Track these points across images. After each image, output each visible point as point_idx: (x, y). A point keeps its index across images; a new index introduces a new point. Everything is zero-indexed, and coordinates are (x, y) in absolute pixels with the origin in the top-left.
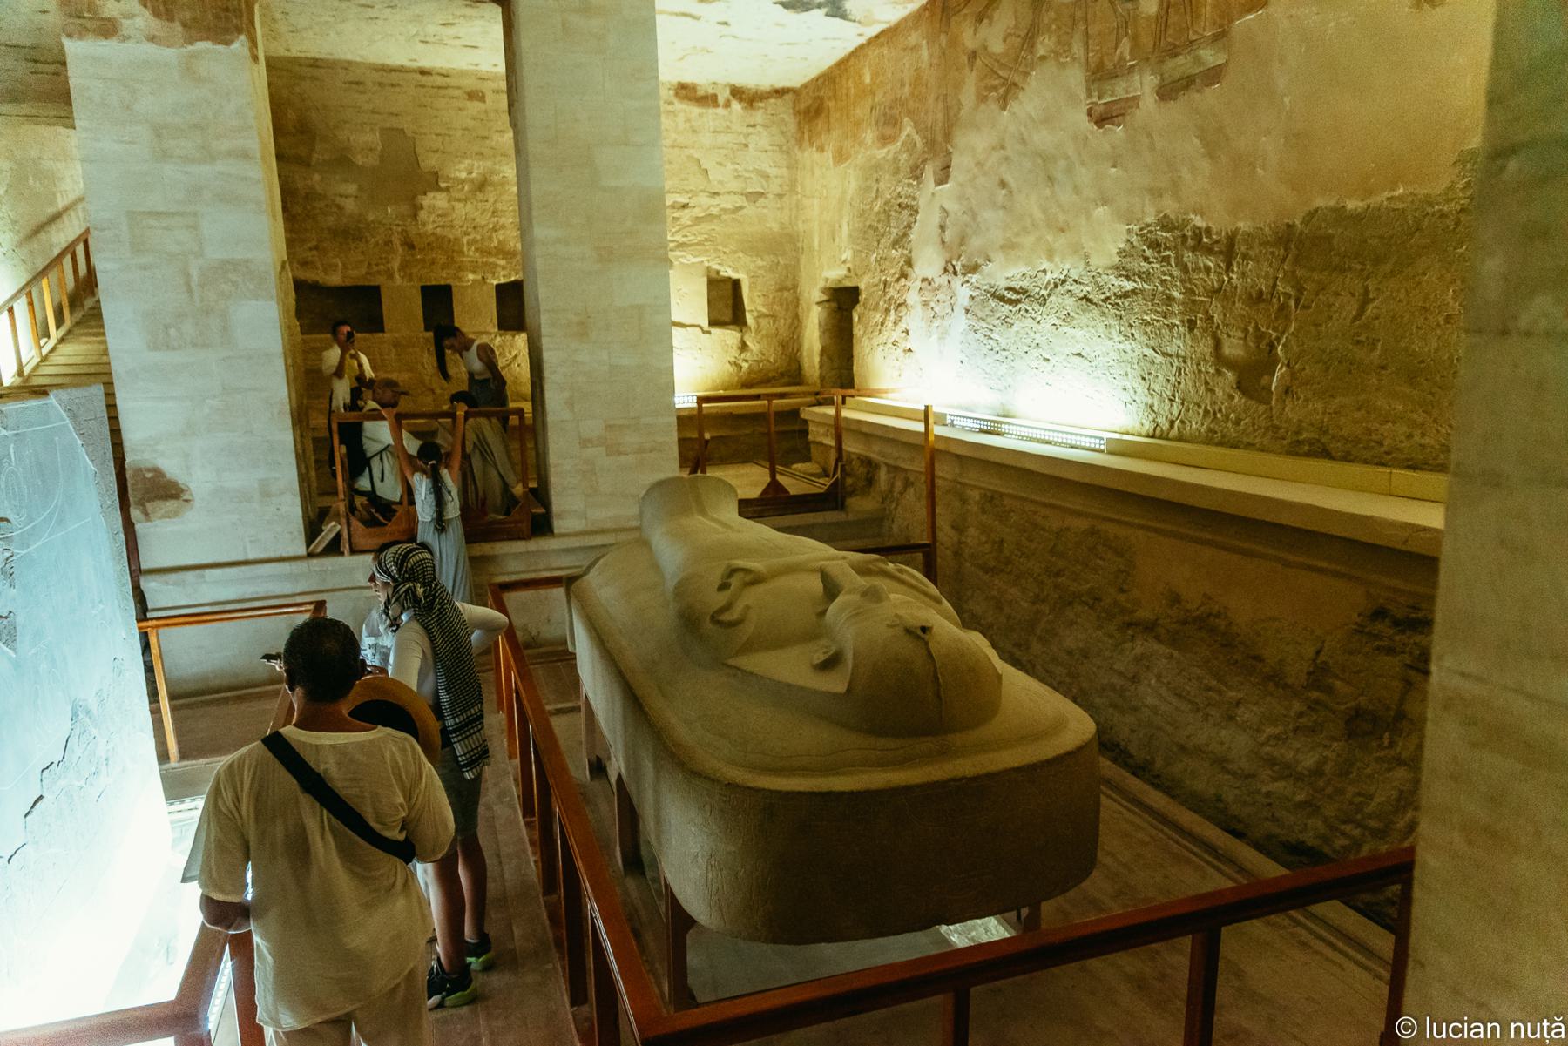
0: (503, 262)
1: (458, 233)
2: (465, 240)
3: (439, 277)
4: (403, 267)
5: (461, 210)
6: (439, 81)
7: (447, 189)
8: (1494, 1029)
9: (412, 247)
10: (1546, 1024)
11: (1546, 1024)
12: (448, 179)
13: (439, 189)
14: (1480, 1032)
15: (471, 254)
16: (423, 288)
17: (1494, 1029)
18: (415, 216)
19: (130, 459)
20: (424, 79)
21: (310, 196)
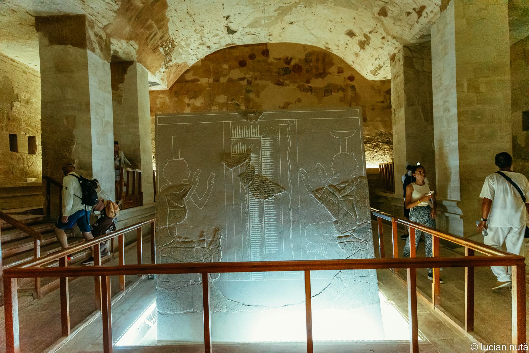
0: (31, 129)
1: (21, 117)
2: (23, 120)
3: (14, 132)
4: (6, 126)
5: (23, 109)
6: (16, 64)
7: (20, 101)
8: (504, 347)
9: (9, 119)
10: (521, 346)
11: (521, 346)
12: (21, 98)
13: (18, 101)
14: (499, 348)
15: (23, 125)
16: (10, 135)
17: (504, 347)
18: (11, 109)
19: (228, 277)
20: (12, 62)
21: (380, 197)
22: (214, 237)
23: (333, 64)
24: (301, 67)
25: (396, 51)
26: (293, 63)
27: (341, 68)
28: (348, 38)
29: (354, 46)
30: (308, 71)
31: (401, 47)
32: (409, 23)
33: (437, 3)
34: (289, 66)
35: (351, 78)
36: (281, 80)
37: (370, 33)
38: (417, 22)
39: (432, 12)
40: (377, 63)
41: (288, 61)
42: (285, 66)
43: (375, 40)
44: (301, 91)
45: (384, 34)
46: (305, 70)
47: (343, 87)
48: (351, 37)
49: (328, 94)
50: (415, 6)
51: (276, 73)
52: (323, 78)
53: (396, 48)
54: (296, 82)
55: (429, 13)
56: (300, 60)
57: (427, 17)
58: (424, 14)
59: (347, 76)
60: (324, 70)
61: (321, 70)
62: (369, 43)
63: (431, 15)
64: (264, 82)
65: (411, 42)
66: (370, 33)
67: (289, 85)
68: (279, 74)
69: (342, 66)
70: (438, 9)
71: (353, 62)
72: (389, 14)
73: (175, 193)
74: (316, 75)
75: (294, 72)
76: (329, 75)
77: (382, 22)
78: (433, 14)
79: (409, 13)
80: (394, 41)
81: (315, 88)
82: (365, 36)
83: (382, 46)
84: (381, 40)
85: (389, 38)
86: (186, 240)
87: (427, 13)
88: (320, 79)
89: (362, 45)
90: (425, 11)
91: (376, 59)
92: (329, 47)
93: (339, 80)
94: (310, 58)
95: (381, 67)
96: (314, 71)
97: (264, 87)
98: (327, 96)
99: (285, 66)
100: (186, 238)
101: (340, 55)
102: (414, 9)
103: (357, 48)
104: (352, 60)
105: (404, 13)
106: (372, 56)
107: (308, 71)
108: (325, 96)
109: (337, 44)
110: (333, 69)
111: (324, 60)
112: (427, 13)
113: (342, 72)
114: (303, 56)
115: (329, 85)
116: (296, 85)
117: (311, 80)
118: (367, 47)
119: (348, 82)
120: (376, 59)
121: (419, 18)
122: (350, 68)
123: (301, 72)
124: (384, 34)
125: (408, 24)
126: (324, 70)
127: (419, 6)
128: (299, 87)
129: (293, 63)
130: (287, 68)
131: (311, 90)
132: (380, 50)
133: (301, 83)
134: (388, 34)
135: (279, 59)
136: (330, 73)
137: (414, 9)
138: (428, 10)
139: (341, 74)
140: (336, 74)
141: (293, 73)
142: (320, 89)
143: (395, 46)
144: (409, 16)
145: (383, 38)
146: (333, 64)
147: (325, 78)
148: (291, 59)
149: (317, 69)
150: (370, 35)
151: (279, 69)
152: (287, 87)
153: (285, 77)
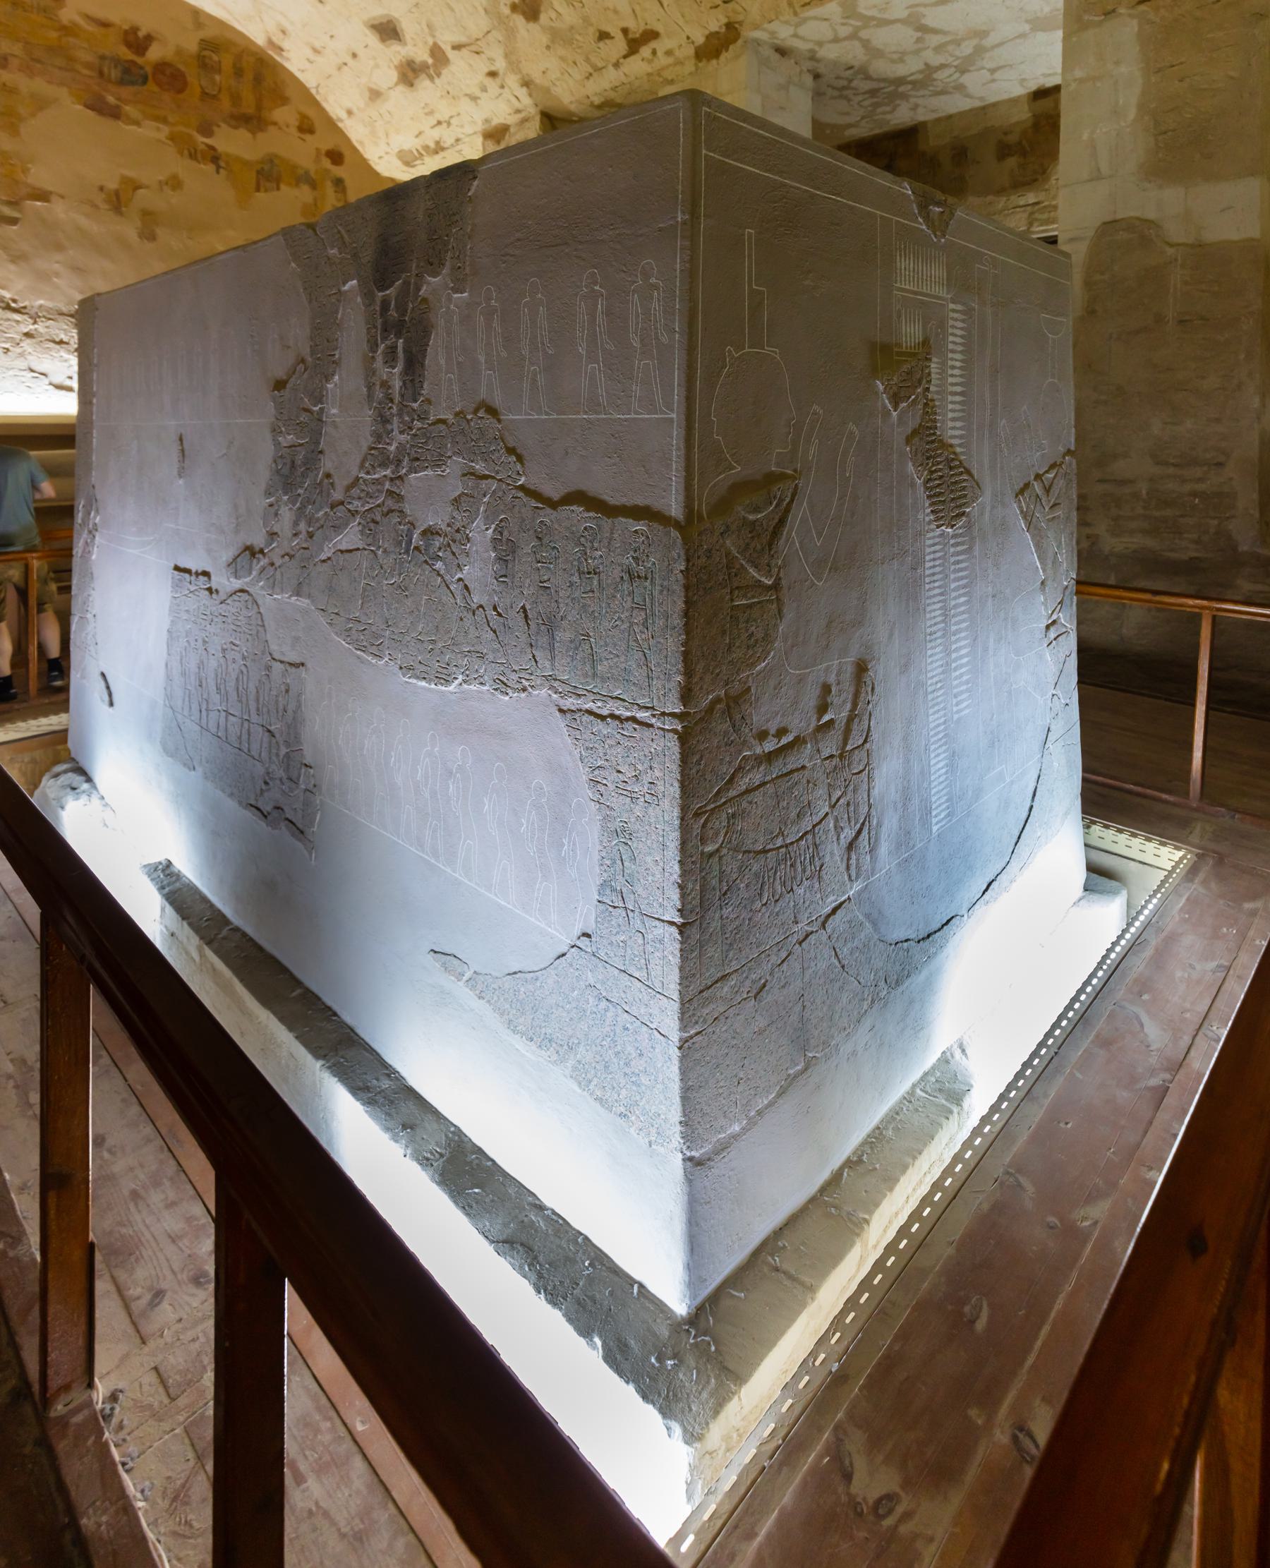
22: (855, 705)
23: (284, 100)
24: (183, 75)
25: (511, 120)
26: (154, 53)
27: (308, 118)
28: (373, 39)
29: (377, 66)
30: (205, 95)
31: (533, 111)
32: (593, 59)
33: (693, 38)
34: (139, 60)
35: (336, 157)
36: (111, 99)
37: (457, 47)
38: (617, 65)
39: (669, 53)
40: (436, 134)
41: (138, 42)
42: (126, 54)
43: (464, 71)
44: (181, 153)
45: (500, 65)
46: (198, 90)
47: (312, 174)
48: (383, 40)
49: (268, 184)
50: (630, 24)
51: (88, 65)
52: (254, 133)
53: (518, 111)
54: (164, 120)
55: (659, 54)
56: (179, 52)
57: (650, 61)
58: (645, 51)
59: (325, 147)
60: (259, 108)
61: (248, 107)
62: (439, 75)
63: (663, 61)
64: (39, 85)
65: (573, 108)
66: (457, 47)
67: (138, 123)
68: (101, 74)
69: (311, 113)
70: (690, 51)
71: (350, 113)
72: (543, 18)
73: (751, 517)
74: (232, 117)
75: (159, 84)
76: (271, 128)
77: (511, 33)
78: (670, 60)
79: (603, 36)
80: (522, 92)
81: (227, 155)
82: (436, 52)
83: (478, 93)
84: (481, 77)
85: (512, 81)
86: (784, 741)
87: (654, 52)
88: (243, 134)
89: (410, 73)
90: (653, 44)
91: (439, 123)
92: (285, 45)
93: (302, 153)
94: (215, 58)
95: (443, 149)
96: (226, 104)
97: (41, 104)
98: (266, 191)
99: (126, 54)
100: (782, 732)
101: (309, 79)
102: (625, 31)
103: (387, 77)
104: (349, 105)
105: (591, 30)
106: (431, 113)
107: (205, 95)
108: (258, 190)
109: (318, 45)
110: (284, 115)
111: (258, 80)
112: (654, 52)
113: (311, 131)
114: (192, 46)
115: (271, 159)
116: (166, 130)
117: (215, 128)
118: (423, 83)
119: (327, 163)
120: (439, 123)
121: (625, 57)
122: (332, 125)
123: (181, 91)
124: (500, 65)
125: (587, 60)
126: (259, 108)
127: (642, 28)
128: (172, 138)
129: (154, 53)
130: (133, 62)
131: (214, 158)
132: (465, 106)
133: (181, 128)
134: (514, 65)
135: (105, 25)
136: (275, 124)
137: (625, 31)
138: (661, 45)
139: (308, 137)
140: (294, 131)
141: (156, 89)
142: (246, 163)
143: (517, 105)
144: (601, 44)
145: (493, 74)
146: (284, 100)
147: (260, 135)
148: (149, 38)
149: (236, 99)
150: (451, 54)
151: (103, 58)
152: (134, 127)
153: (126, 91)
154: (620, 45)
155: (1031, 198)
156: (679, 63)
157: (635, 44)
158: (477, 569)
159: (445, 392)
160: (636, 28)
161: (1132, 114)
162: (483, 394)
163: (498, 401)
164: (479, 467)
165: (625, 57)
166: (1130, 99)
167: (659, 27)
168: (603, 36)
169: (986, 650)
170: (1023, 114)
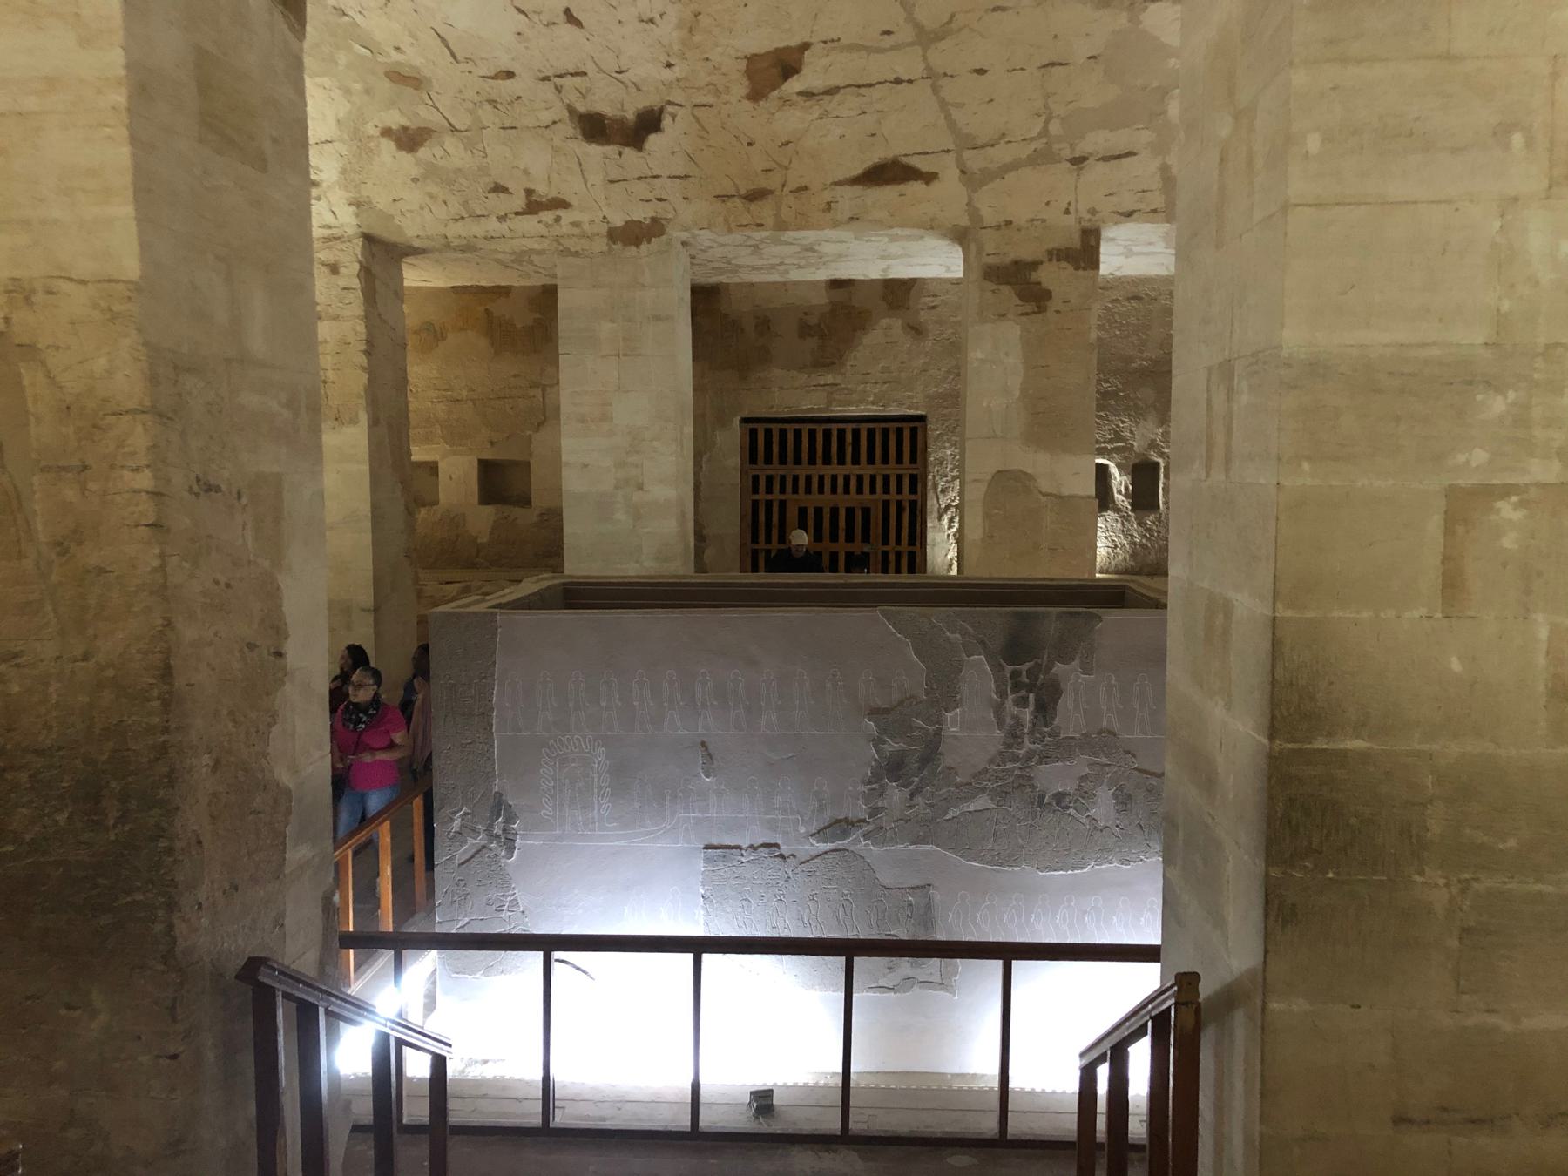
39: (576, 224)
57: (547, 225)
58: (547, 216)
63: (565, 228)
70: (604, 229)
87: (558, 219)
90: (560, 212)
121: (517, 214)
137: (529, 192)
144: (491, 196)
154: (519, 202)
155: (829, 379)
156: (590, 238)
157: (534, 206)
158: (1103, 806)
159: (1070, 717)
160: (543, 190)
161: (1017, 394)
162: (1104, 724)
163: (1116, 727)
164: (1103, 760)
165: (517, 214)
166: (1015, 382)
167: (574, 201)
168: (499, 189)
169: (562, 805)
170: (821, 299)
